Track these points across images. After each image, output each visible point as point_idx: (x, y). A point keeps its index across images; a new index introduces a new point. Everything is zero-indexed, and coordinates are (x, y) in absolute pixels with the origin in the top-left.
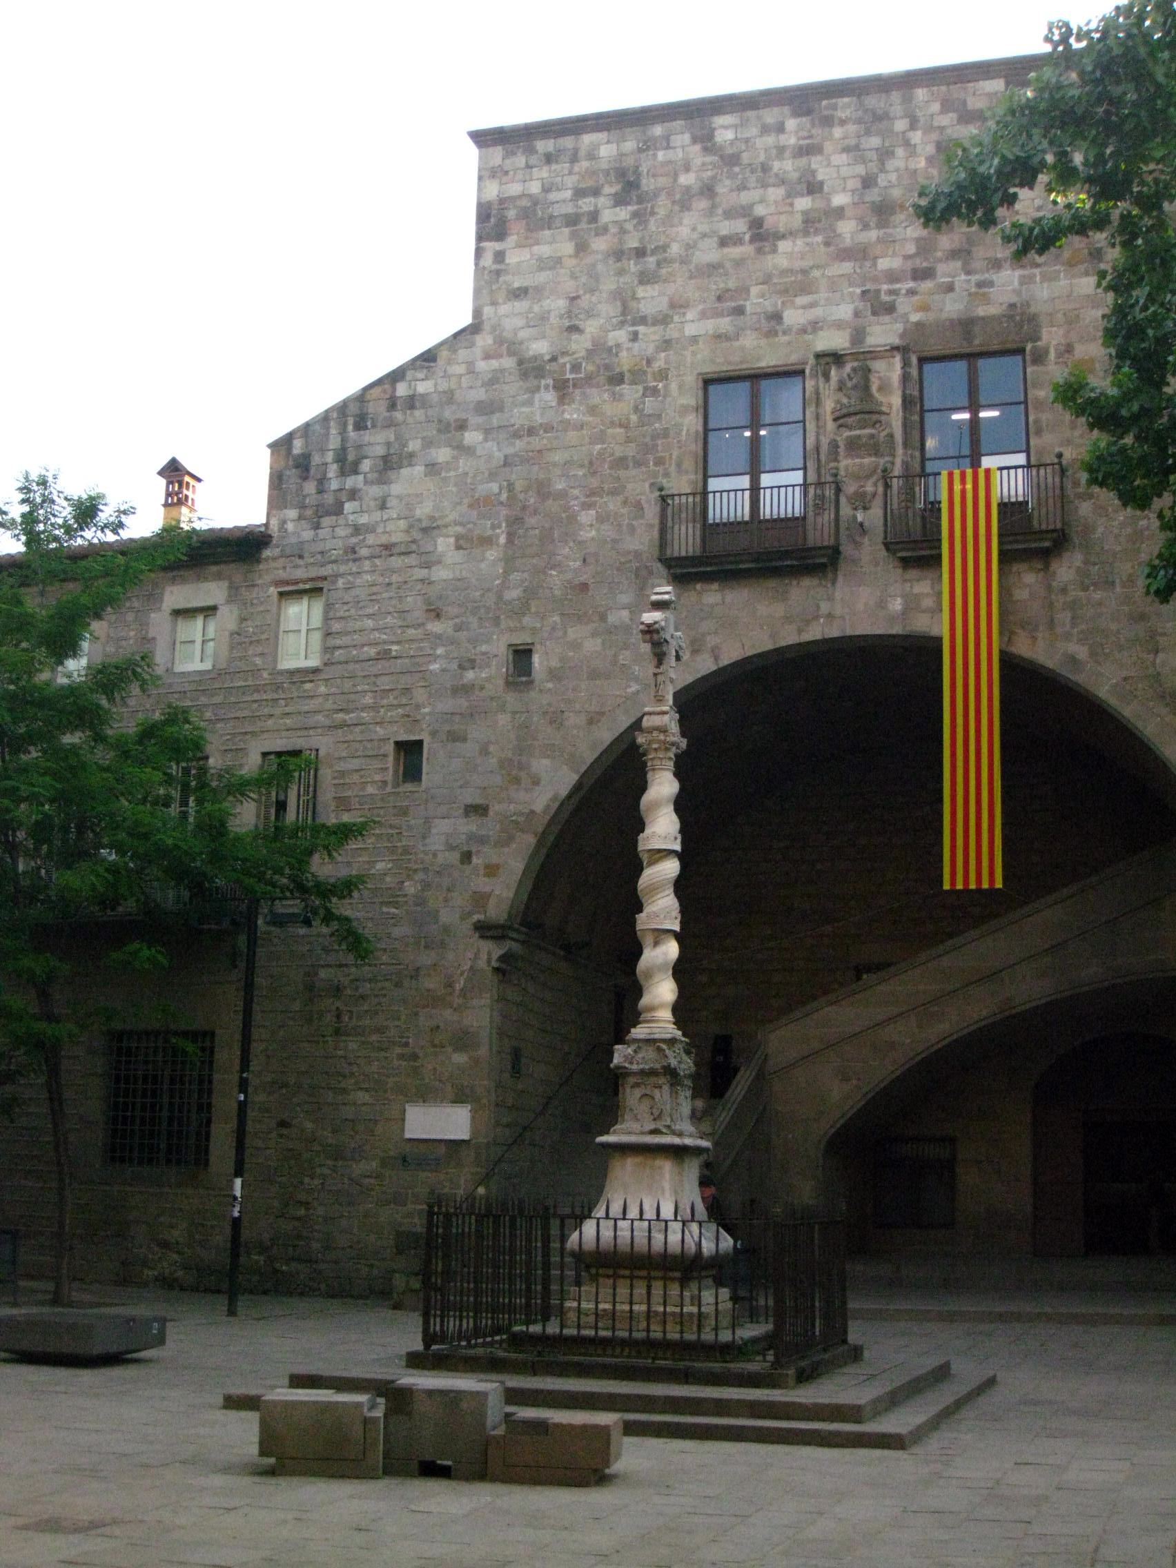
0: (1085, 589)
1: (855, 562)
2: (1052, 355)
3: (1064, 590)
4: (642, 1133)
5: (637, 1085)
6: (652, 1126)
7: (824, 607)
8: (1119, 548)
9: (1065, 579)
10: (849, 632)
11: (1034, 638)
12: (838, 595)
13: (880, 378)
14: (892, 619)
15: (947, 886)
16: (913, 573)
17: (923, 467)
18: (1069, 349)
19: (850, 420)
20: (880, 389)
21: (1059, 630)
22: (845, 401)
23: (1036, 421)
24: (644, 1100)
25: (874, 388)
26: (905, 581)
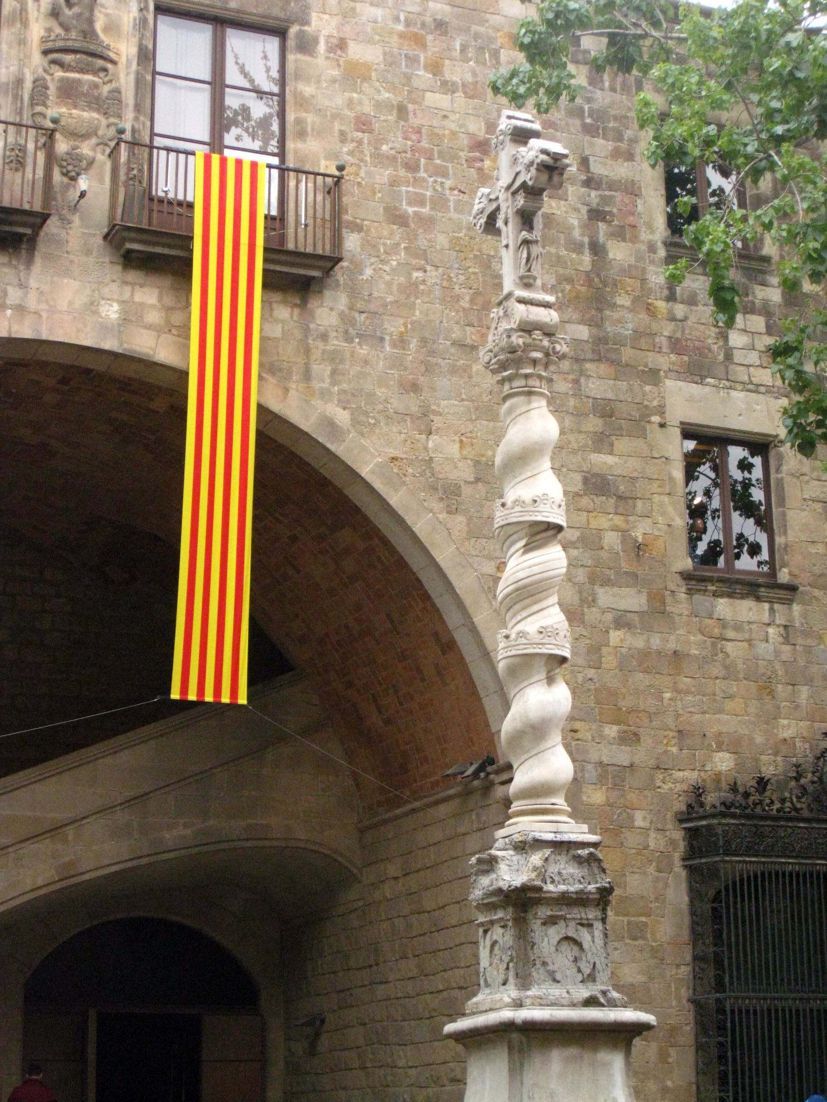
0: (349, 340)
1: (59, 243)
2: (322, 47)
3: (324, 337)
4: (573, 1005)
5: (552, 921)
6: (585, 993)
7: (14, 295)
8: (390, 299)
9: (326, 322)
10: (45, 336)
11: (286, 390)
12: (33, 283)
13: (107, 15)
14: (105, 328)
15: (175, 695)
16: (133, 276)
17: (151, 140)
18: (342, 45)
19: (68, 58)
20: (107, 29)
21: (316, 384)
22: (58, 30)
23: (298, 121)
24: (565, 946)
25: (99, 26)
26: (125, 283)
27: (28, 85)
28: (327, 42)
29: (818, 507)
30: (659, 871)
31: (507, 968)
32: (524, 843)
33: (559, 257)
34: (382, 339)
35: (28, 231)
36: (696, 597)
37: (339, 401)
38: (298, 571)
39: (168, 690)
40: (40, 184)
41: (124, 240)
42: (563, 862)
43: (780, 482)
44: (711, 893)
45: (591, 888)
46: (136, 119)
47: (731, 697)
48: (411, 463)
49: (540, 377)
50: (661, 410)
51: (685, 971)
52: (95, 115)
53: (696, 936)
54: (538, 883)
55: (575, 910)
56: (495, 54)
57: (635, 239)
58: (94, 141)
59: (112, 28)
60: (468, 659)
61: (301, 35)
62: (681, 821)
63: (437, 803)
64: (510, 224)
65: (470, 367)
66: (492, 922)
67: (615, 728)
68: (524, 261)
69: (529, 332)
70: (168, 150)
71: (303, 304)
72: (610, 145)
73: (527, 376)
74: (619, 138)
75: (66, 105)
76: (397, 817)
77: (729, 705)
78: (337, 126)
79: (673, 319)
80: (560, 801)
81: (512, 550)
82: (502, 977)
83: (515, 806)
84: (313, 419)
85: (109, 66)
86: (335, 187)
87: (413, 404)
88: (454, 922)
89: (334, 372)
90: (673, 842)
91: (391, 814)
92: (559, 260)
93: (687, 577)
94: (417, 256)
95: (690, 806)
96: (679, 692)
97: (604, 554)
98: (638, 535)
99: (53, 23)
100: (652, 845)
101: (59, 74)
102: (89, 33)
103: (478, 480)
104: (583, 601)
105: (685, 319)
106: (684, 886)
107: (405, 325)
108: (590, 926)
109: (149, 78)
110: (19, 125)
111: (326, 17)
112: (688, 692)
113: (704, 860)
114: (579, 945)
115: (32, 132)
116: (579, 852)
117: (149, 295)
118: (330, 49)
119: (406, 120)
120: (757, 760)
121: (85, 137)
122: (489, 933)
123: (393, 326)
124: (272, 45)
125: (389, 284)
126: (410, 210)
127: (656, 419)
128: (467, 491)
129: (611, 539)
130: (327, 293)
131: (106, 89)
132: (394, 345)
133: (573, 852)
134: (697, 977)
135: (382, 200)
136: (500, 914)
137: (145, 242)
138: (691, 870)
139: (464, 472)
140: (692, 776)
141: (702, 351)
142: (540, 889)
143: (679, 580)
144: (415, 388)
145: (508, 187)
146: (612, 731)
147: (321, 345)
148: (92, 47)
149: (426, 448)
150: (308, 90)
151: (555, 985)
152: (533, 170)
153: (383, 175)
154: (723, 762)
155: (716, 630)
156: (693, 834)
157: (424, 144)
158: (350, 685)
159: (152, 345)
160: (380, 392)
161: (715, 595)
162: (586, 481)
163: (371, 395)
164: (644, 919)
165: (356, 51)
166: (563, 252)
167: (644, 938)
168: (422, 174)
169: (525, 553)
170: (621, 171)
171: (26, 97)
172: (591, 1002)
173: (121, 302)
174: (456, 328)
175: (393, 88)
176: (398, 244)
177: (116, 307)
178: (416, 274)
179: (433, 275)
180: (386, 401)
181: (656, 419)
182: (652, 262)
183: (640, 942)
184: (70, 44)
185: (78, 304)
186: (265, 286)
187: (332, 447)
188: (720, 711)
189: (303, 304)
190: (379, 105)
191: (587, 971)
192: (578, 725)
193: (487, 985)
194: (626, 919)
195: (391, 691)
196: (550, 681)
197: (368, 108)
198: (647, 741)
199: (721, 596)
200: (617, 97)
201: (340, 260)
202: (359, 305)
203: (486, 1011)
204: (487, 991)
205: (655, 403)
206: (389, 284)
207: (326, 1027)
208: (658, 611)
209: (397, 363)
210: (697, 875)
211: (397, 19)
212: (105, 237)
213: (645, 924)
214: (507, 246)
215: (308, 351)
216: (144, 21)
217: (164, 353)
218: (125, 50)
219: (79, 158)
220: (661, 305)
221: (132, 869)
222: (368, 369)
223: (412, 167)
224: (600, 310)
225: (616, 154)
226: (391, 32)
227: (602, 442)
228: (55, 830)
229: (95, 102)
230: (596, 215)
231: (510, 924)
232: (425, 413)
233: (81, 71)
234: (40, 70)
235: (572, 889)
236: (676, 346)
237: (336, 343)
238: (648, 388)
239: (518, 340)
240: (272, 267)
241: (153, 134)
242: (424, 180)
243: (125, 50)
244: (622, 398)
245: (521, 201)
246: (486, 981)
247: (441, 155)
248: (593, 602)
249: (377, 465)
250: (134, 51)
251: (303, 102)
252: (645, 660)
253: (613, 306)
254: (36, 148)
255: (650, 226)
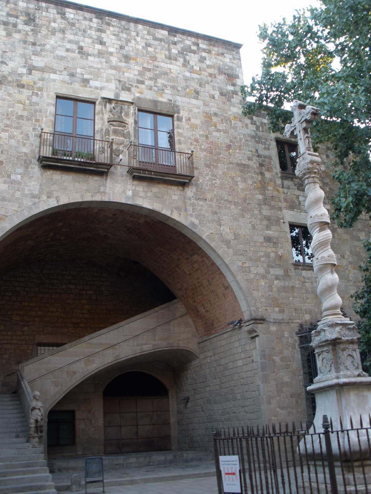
1: (113, 173)
2: (184, 120)
3: (190, 199)
4: (354, 377)
11: (180, 214)
12: (107, 185)
14: (128, 198)
16: (136, 182)
19: (115, 123)
22: (112, 116)
26: (133, 185)
27: (104, 130)
28: (185, 118)
30: (292, 349)
31: (331, 366)
32: (332, 324)
33: (252, 176)
35: (106, 170)
36: (296, 270)
37: (195, 217)
38: (180, 269)
40: (109, 158)
41: (133, 172)
42: (344, 330)
44: (307, 354)
45: (355, 338)
46: (134, 139)
47: (308, 299)
48: (216, 234)
50: (283, 218)
51: (301, 377)
53: (304, 367)
54: (340, 337)
56: (231, 122)
57: (272, 171)
60: (234, 290)
61: (178, 117)
62: (297, 334)
64: (301, 132)
65: (230, 207)
66: (322, 352)
67: (278, 309)
68: (307, 143)
72: (263, 146)
73: (313, 177)
74: (265, 144)
75: (115, 136)
76: (210, 339)
77: (308, 301)
78: (189, 141)
79: (284, 193)
80: (339, 311)
81: (314, 233)
82: (328, 368)
83: (324, 314)
84: (188, 222)
85: (126, 125)
86: (191, 157)
87: (216, 217)
88: (232, 367)
89: (193, 209)
91: (208, 338)
92: (252, 177)
94: (214, 176)
95: (299, 330)
96: (294, 298)
97: (271, 259)
98: (279, 253)
99: (110, 114)
100: (290, 341)
101: (112, 128)
103: (235, 239)
104: (266, 272)
105: (287, 193)
106: (299, 353)
108: (355, 350)
110: (103, 141)
112: (296, 298)
113: (304, 345)
114: (353, 357)
115: (106, 143)
116: (349, 327)
118: (186, 120)
119: (208, 139)
120: (316, 316)
121: (121, 144)
122: (321, 355)
127: (282, 221)
128: (232, 242)
129: (272, 255)
130: (190, 187)
131: (126, 131)
133: (347, 327)
135: (203, 161)
136: (325, 349)
138: (301, 348)
139: (231, 237)
141: (293, 202)
142: (340, 339)
143: (292, 266)
144: (216, 213)
145: (299, 122)
146: (277, 309)
147: (189, 201)
148: (121, 121)
151: (348, 371)
152: (310, 114)
155: (303, 280)
158: (195, 301)
160: (206, 214)
162: (264, 238)
163: (204, 215)
164: (289, 363)
165: (193, 121)
166: (253, 175)
167: (289, 368)
169: (319, 232)
170: (266, 153)
171: (104, 134)
173: (132, 190)
175: (204, 131)
176: (208, 173)
178: (214, 181)
181: (282, 221)
182: (277, 178)
183: (289, 369)
184: (115, 119)
185: (120, 191)
187: (194, 230)
188: (305, 303)
190: (200, 135)
191: (356, 365)
192: (267, 308)
193: (321, 372)
194: (284, 363)
195: (208, 302)
198: (286, 312)
199: (303, 270)
200: (264, 133)
201: (193, 177)
203: (324, 381)
204: (322, 375)
205: (281, 216)
206: (207, 184)
207: (190, 400)
208: (287, 275)
212: (127, 172)
213: (290, 364)
214: (301, 139)
215: (185, 203)
218: (130, 121)
219: (119, 150)
220: (281, 189)
221: (135, 357)
222: (203, 208)
224: (264, 191)
225: (265, 148)
227: (268, 228)
229: (124, 136)
230: (261, 165)
231: (331, 351)
232: (219, 220)
234: (107, 126)
235: (350, 339)
236: (286, 200)
238: (279, 212)
239: (310, 166)
244: (272, 215)
245: (304, 125)
246: (320, 371)
248: (269, 273)
250: (133, 121)
252: (284, 289)
253: (268, 190)
254: (108, 148)
255: (275, 168)
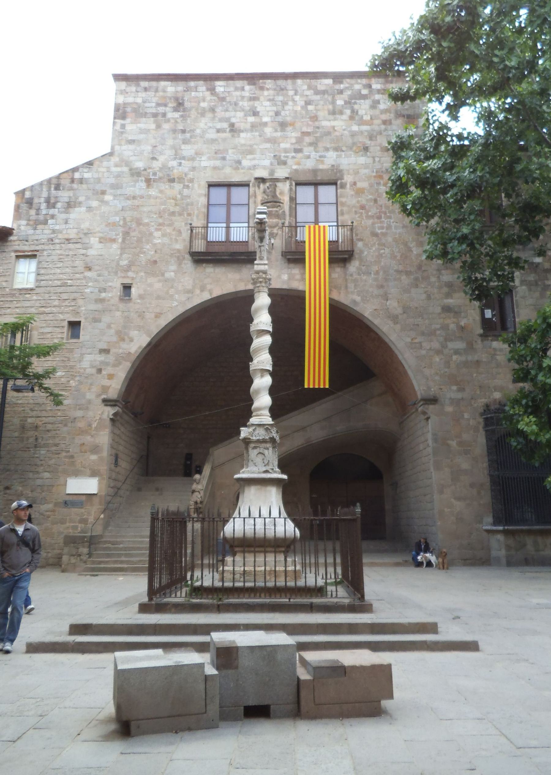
2: (348, 186)
3: (351, 275)
4: (259, 473)
5: (255, 448)
8: (373, 260)
11: (340, 293)
15: (306, 386)
16: (292, 265)
17: (296, 224)
18: (355, 183)
20: (280, 194)
21: (350, 290)
22: (266, 197)
23: (342, 210)
24: (260, 455)
25: (278, 193)
26: (289, 268)
29: (532, 307)
34: (371, 273)
39: (304, 385)
43: (516, 301)
49: (263, 286)
51: (486, 465)
52: (277, 220)
53: (489, 453)
55: (263, 445)
58: (277, 228)
59: (282, 193)
61: (341, 183)
62: (482, 416)
63: (412, 414)
69: (259, 273)
70: (300, 227)
71: (345, 266)
73: (258, 287)
78: (354, 210)
85: (281, 204)
89: (355, 286)
90: (479, 423)
93: (481, 335)
95: (484, 410)
98: (462, 324)
100: (471, 423)
102: (275, 196)
103: (404, 313)
107: (378, 268)
109: (294, 206)
111: (349, 176)
114: (264, 455)
117: (296, 271)
118: (351, 186)
121: (274, 227)
123: (375, 268)
124: (334, 187)
125: (372, 256)
126: (379, 231)
128: (400, 317)
129: (452, 326)
131: (281, 211)
132: (375, 274)
134: (490, 466)
137: (292, 255)
140: (484, 401)
142: (250, 439)
144: (382, 287)
146: (455, 388)
147: (350, 278)
148: (275, 200)
149: (386, 305)
150: (343, 200)
153: (370, 222)
154: (497, 395)
156: (486, 419)
157: (383, 209)
159: (296, 285)
160: (371, 290)
161: (492, 341)
164: (469, 448)
168: (383, 219)
172: (266, 472)
173: (287, 274)
174: (395, 266)
177: (286, 275)
179: (387, 251)
180: (372, 292)
186: (330, 262)
189: (345, 266)
196: (262, 376)
197: (364, 202)
202: (363, 264)
206: (372, 256)
209: (376, 280)
210: (489, 434)
211: (373, 172)
215: (346, 280)
216: (291, 189)
217: (301, 288)
223: (379, 218)
226: (371, 176)
228: (303, 429)
229: (278, 216)
233: (272, 208)
237: (355, 276)
240: (332, 257)
241: (296, 222)
242: (383, 221)
243: (286, 199)
247: (389, 212)
249: (371, 312)
251: (343, 204)
252: (466, 364)
